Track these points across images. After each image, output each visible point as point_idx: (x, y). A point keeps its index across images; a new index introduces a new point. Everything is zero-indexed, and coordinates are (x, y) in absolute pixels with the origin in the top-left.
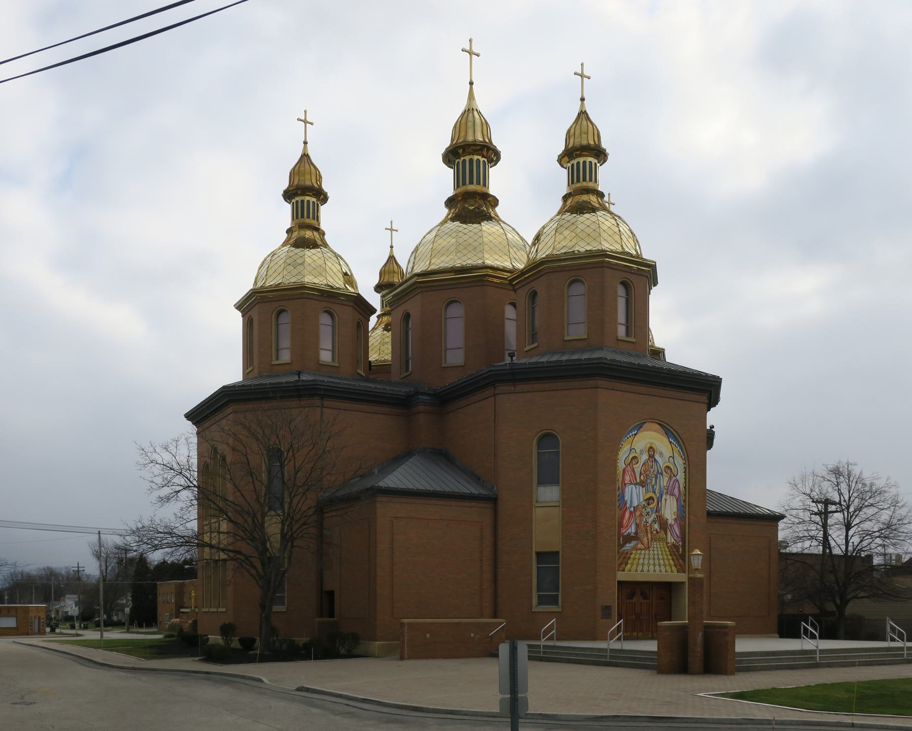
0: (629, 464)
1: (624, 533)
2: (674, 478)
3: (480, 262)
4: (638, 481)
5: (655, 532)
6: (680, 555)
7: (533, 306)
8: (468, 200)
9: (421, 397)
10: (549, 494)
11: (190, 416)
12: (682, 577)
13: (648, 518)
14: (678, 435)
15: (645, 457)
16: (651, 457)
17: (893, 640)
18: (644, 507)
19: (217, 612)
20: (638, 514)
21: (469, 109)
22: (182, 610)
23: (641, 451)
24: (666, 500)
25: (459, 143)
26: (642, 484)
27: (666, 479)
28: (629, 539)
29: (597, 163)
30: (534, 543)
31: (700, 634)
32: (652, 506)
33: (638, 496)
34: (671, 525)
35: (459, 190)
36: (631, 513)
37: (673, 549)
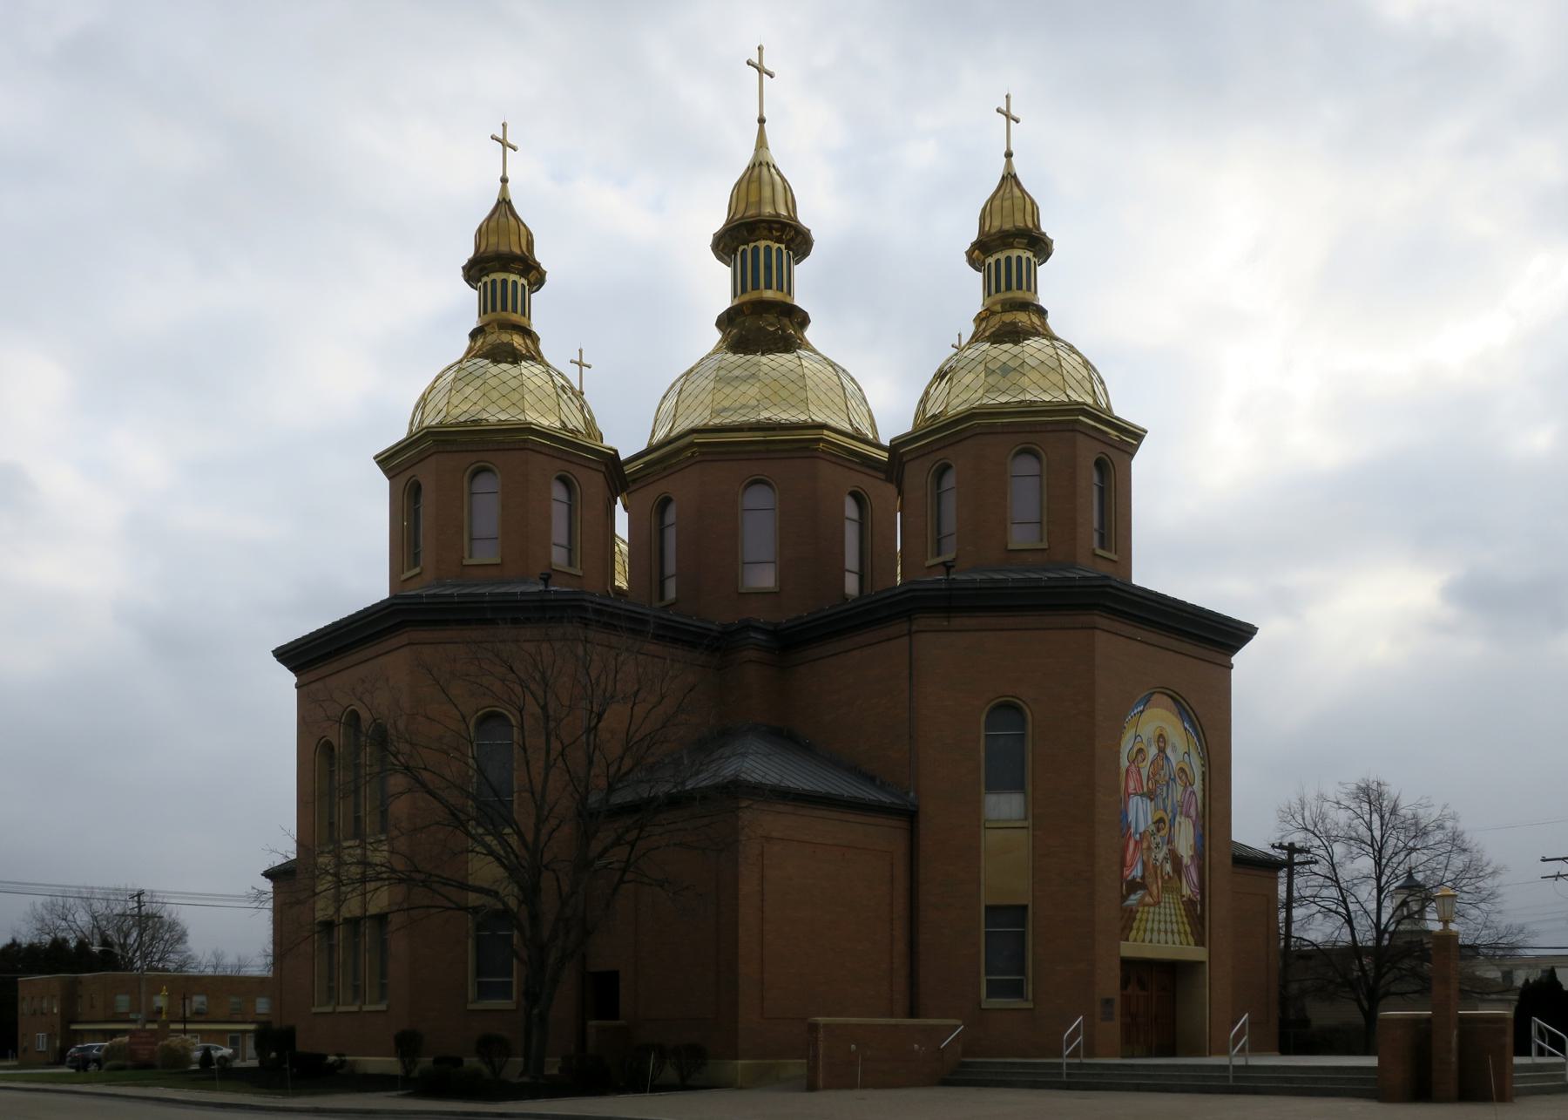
0: (1133, 762)
1: (1128, 876)
2: (1190, 789)
3: (803, 417)
4: (1145, 789)
5: (1166, 877)
6: (1197, 918)
7: (939, 491)
8: (764, 315)
9: (752, 635)
10: (1004, 807)
11: (290, 655)
12: (1199, 954)
13: (1159, 852)
14: (1196, 715)
15: (1153, 751)
16: (1162, 750)
17: (1541, 1052)
18: (1153, 834)
19: (333, 1013)
20: (1145, 845)
21: (754, 164)
22: (74, 1027)
23: (1149, 741)
24: (1180, 823)
25: (736, 221)
26: (1151, 796)
27: (1180, 789)
28: (1133, 886)
29: (1031, 257)
30: (983, 887)
31: (1455, 1033)
32: (1162, 833)
33: (1145, 814)
34: (1187, 867)
35: (746, 298)
36: (1136, 842)
37: (1189, 904)
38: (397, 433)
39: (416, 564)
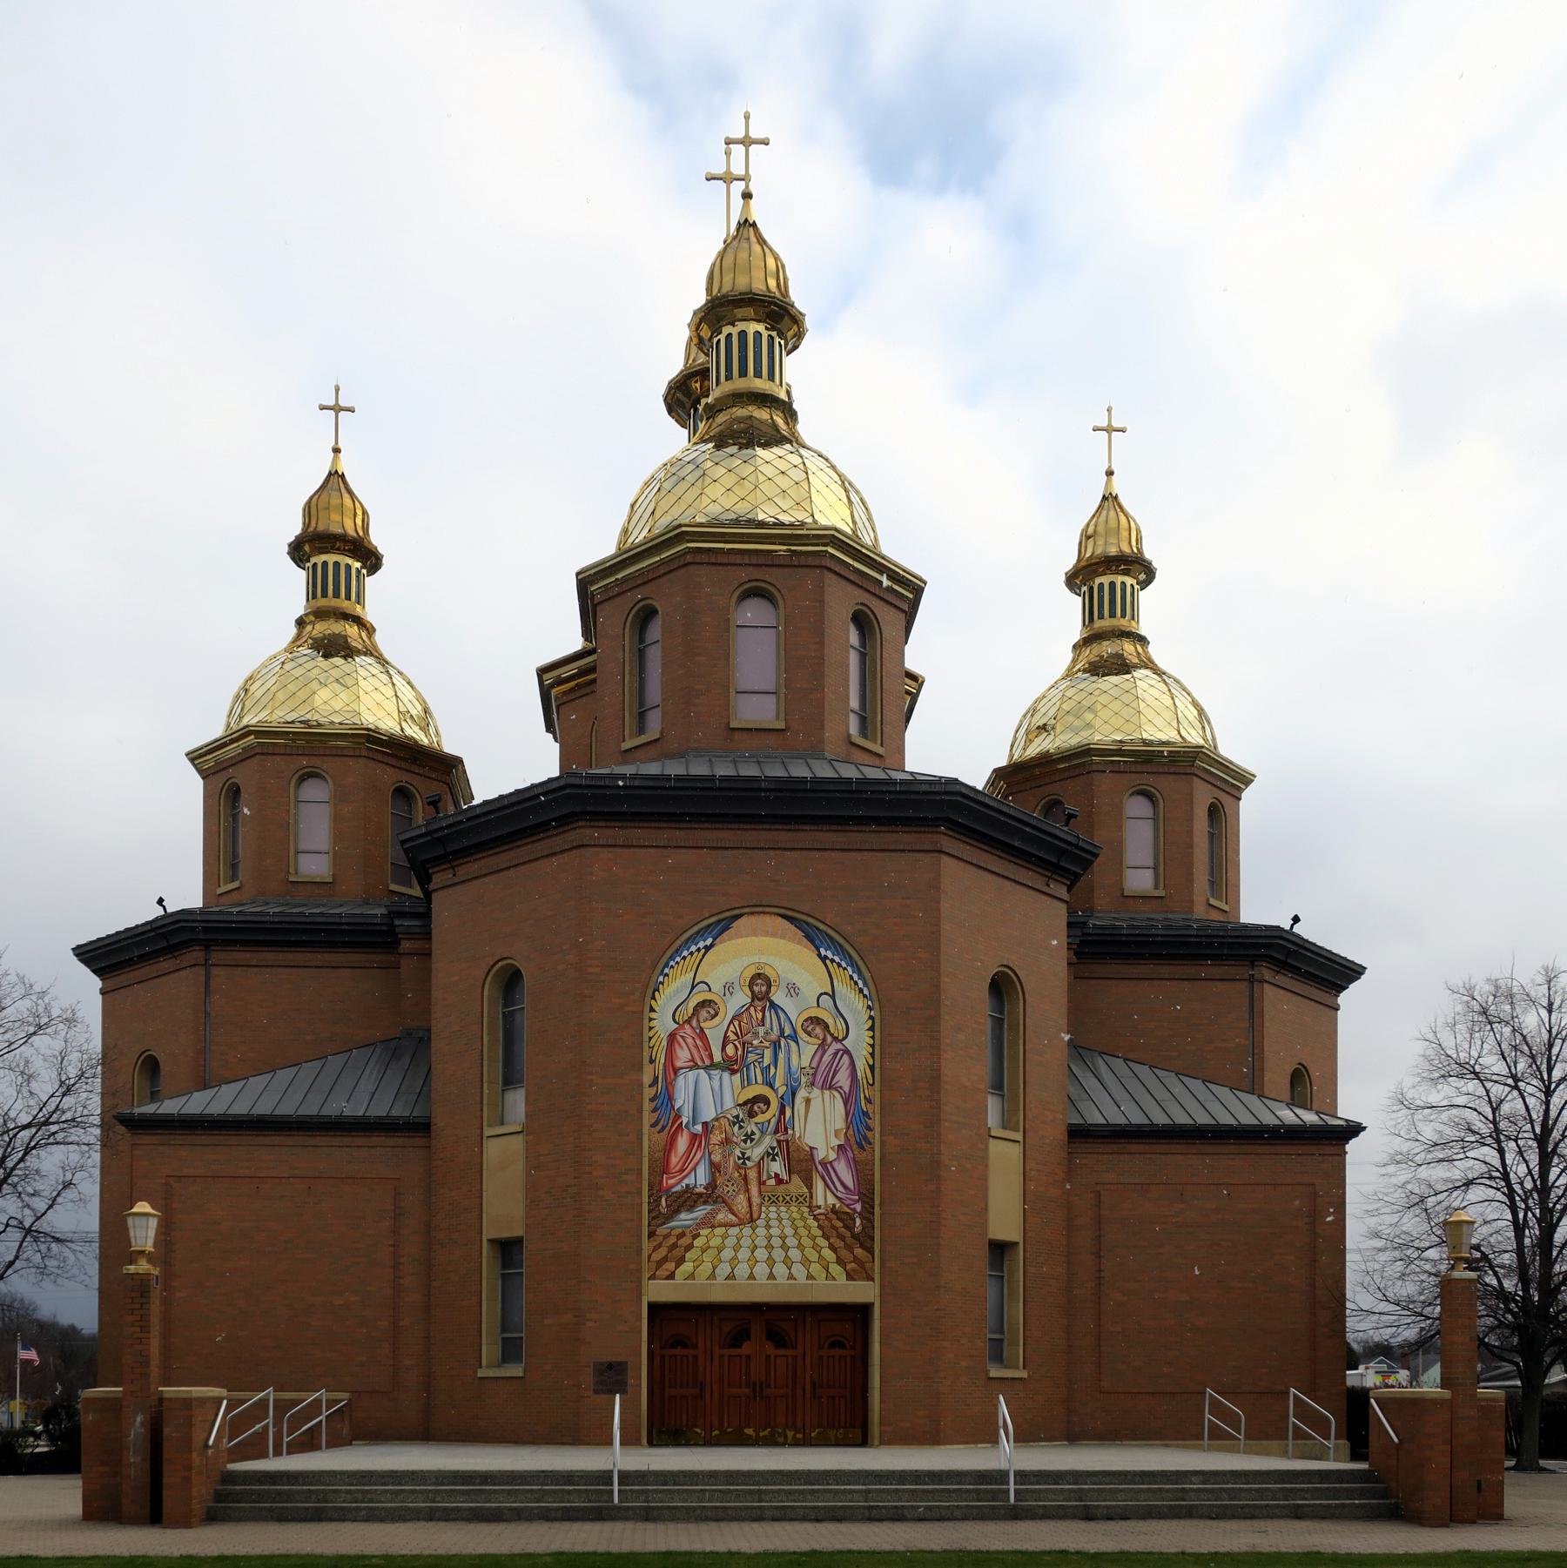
28: (689, 1199)
29: (1135, 584)
38: (212, 729)
39: (234, 878)
